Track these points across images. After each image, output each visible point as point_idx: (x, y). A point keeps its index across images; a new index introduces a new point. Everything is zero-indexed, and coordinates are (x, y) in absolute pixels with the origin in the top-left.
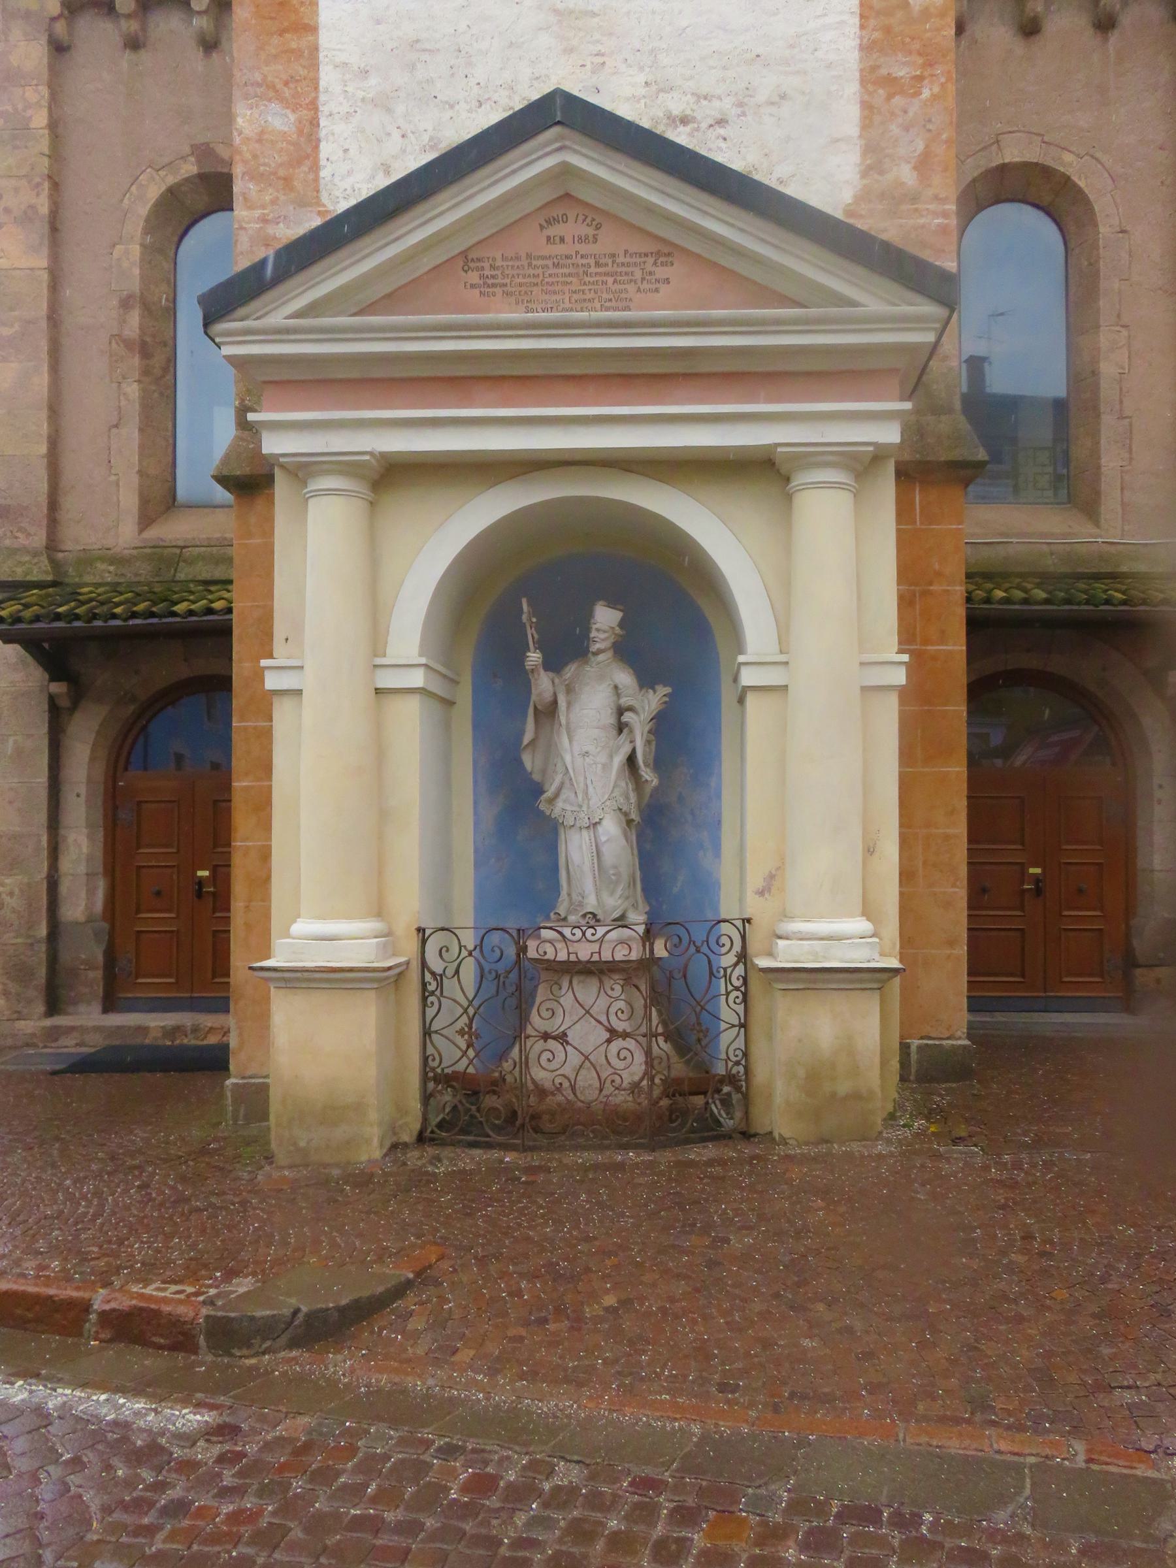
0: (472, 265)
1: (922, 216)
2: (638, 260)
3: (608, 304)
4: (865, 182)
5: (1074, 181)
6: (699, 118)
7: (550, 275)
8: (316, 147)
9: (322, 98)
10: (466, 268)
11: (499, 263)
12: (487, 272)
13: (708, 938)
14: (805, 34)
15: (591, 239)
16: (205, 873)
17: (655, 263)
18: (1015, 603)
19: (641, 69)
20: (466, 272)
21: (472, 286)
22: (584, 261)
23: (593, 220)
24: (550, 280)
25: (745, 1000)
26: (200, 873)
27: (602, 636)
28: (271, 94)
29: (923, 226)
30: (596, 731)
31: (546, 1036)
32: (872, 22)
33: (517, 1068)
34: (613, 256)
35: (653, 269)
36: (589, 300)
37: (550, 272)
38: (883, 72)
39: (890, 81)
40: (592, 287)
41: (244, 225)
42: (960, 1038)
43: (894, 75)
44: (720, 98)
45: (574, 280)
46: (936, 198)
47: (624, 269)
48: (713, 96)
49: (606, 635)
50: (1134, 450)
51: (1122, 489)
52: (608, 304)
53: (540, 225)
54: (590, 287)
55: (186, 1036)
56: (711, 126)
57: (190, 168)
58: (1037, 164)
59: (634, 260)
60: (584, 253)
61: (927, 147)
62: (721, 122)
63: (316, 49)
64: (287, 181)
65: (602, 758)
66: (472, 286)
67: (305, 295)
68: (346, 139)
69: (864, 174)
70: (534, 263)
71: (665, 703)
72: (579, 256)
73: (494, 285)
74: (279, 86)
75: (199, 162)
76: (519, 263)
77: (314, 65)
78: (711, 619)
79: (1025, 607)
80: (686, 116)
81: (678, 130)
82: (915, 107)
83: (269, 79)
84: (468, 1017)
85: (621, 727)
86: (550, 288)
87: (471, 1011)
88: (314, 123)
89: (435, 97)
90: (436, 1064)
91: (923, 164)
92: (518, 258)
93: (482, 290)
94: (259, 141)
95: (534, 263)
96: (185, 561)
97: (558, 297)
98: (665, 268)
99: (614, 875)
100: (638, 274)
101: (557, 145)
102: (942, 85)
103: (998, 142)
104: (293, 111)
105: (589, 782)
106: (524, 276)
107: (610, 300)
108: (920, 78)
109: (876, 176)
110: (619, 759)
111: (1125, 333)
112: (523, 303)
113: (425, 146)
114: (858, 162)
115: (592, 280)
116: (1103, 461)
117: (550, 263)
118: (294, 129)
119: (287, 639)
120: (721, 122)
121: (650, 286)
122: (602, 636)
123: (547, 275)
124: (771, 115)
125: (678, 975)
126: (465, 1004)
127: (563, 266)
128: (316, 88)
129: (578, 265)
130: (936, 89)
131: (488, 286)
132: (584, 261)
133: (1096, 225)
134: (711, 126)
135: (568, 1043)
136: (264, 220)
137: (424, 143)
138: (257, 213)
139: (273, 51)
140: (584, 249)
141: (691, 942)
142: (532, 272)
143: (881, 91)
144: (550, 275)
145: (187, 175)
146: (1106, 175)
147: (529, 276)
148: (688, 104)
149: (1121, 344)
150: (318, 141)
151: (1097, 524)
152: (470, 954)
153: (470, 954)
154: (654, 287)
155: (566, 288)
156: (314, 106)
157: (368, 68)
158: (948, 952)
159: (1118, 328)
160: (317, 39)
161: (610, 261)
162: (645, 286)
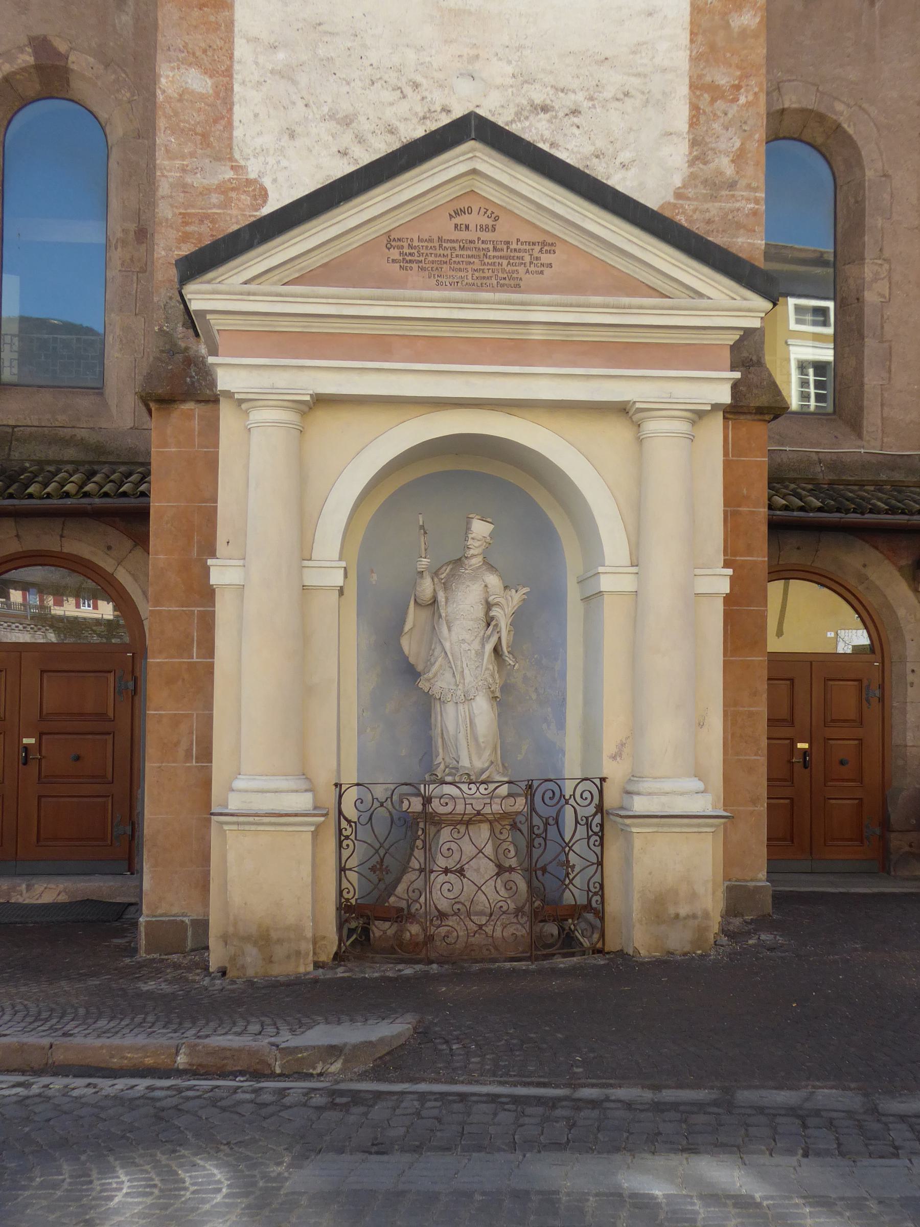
0: (393, 243)
1: (738, 201)
2: (527, 247)
3: (502, 282)
4: (692, 170)
5: (843, 128)
6: (557, 108)
7: (457, 256)
8: (230, 110)
9: (237, 67)
10: (389, 246)
11: (416, 243)
12: (406, 250)
13: (574, 792)
14: (645, 43)
15: (490, 227)
16: (32, 741)
17: (541, 251)
18: (793, 510)
19: (509, 62)
20: (389, 249)
21: (394, 261)
22: (484, 246)
23: (493, 213)
24: (457, 260)
25: (602, 845)
26: (26, 741)
27: (477, 544)
28: (191, 59)
29: (738, 210)
30: (471, 623)
31: (446, 871)
32: (700, 38)
33: (423, 896)
34: (508, 243)
35: (539, 255)
36: (488, 278)
37: (457, 253)
38: (708, 79)
39: (715, 92)
40: (491, 267)
41: (166, 173)
42: (760, 881)
43: (717, 83)
44: (574, 92)
45: (476, 261)
46: (749, 187)
47: (517, 254)
48: (569, 90)
49: (480, 543)
50: (893, 370)
51: (882, 405)
52: (502, 282)
53: (450, 215)
54: (489, 267)
55: (21, 895)
56: (567, 115)
57: (27, 58)
58: (811, 111)
59: (524, 247)
60: (485, 239)
61: (742, 144)
62: (575, 112)
63: (232, 22)
64: (205, 136)
65: (476, 645)
66: (394, 261)
67: (263, 263)
68: (256, 105)
69: (692, 163)
70: (444, 245)
71: (524, 599)
72: (480, 242)
73: (411, 261)
74: (198, 53)
75: (36, 54)
76: (432, 245)
77: (229, 40)
78: (560, 531)
79: (802, 514)
80: (546, 106)
81: (539, 116)
82: (733, 110)
83: (190, 46)
84: (380, 856)
85: (489, 621)
86: (458, 266)
87: (382, 852)
88: (229, 89)
89: (335, 74)
90: (350, 896)
91: (739, 158)
92: (431, 240)
93: (402, 264)
94: (180, 100)
95: (444, 245)
96: (17, 440)
97: (462, 274)
98: (549, 255)
99: (483, 742)
100: (527, 259)
101: (470, 155)
102: (755, 94)
103: (779, 88)
104: (211, 77)
105: (465, 665)
106: (436, 255)
107: (505, 279)
108: (737, 87)
109: (701, 166)
110: (489, 647)
111: (886, 266)
112: (434, 278)
113: (324, 116)
114: (687, 153)
115: (490, 261)
116: (866, 380)
117: (456, 245)
118: (211, 92)
119: (228, 543)
120: (575, 112)
121: (537, 269)
122: (477, 544)
123: (454, 255)
124: (616, 109)
125: (551, 821)
126: (377, 846)
127: (469, 249)
128: (231, 57)
129: (479, 249)
130: (751, 98)
131: (407, 262)
132: (484, 246)
133: (862, 168)
134: (567, 115)
135: (465, 877)
136: (184, 170)
137: (324, 113)
138: (178, 163)
139: (194, 23)
140: (485, 236)
141: (562, 796)
142: (442, 252)
143: (706, 96)
144: (457, 256)
145: (24, 65)
146: (872, 124)
147: (440, 255)
148: (548, 95)
149: (882, 276)
150: (232, 104)
151: (860, 436)
152: (382, 805)
153: (382, 805)
154: (540, 269)
155: (469, 267)
156: (229, 73)
157: (277, 44)
158: (751, 809)
159: (880, 262)
160: (233, 15)
161: (505, 247)
162: (532, 268)
